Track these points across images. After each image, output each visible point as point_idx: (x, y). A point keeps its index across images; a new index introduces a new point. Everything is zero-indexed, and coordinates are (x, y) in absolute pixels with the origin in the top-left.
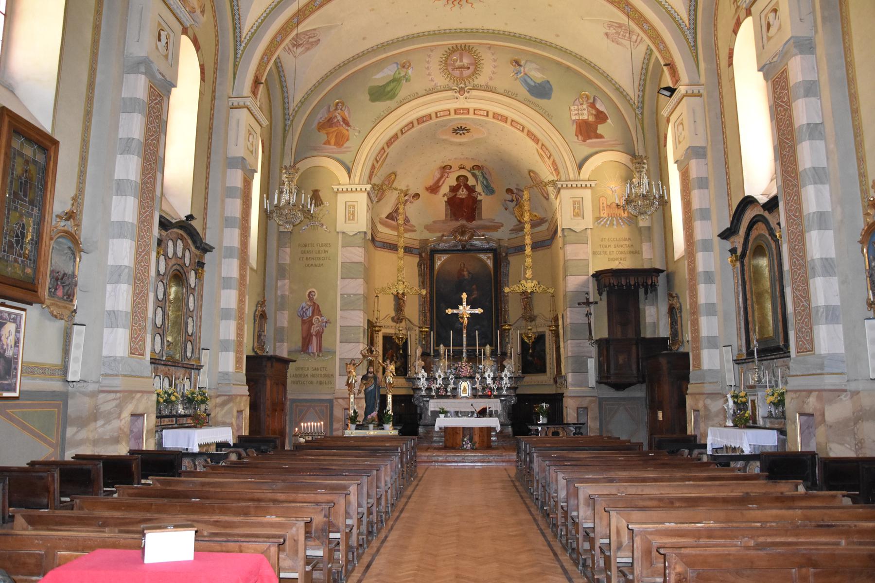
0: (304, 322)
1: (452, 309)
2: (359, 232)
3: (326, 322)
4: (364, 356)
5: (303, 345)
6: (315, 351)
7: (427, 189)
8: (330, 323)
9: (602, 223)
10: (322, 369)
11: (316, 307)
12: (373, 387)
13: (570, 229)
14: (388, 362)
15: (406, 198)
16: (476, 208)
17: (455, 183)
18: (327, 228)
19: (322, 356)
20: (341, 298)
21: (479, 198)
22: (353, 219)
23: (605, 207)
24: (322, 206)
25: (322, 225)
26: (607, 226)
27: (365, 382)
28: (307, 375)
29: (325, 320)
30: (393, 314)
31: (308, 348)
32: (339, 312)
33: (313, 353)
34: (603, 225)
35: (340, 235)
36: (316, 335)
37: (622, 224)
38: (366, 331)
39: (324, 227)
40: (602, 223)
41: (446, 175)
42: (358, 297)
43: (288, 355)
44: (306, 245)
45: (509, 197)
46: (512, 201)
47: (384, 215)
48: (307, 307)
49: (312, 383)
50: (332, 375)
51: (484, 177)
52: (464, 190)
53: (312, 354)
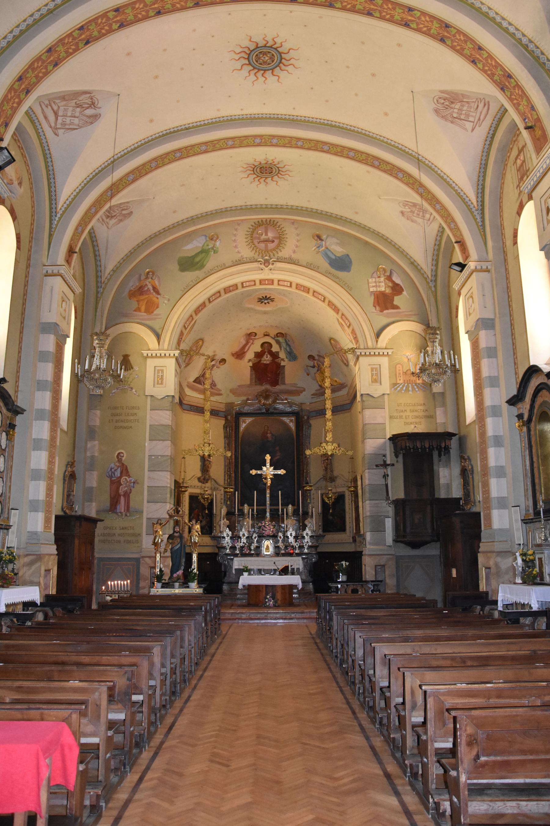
0: (112, 482)
1: (256, 470)
2: (167, 396)
3: (134, 483)
4: (171, 516)
5: (111, 505)
6: (123, 511)
7: (233, 355)
8: (138, 483)
9: (399, 389)
10: (130, 528)
11: (124, 468)
12: (177, 547)
13: (368, 394)
14: (194, 522)
15: (213, 363)
16: (279, 373)
17: (259, 349)
18: (136, 391)
19: (130, 516)
20: (149, 459)
21: (283, 364)
22: (162, 383)
23: (401, 374)
24: (132, 370)
25: (132, 388)
26: (403, 392)
27: (170, 541)
28: (114, 534)
29: (132, 481)
30: (199, 474)
31: (116, 508)
32: (147, 473)
33: (121, 513)
34: (398, 391)
35: (149, 398)
36: (124, 496)
37: (417, 390)
38: (173, 491)
39: (134, 390)
40: (399, 389)
41: (251, 341)
42: (165, 458)
43: (97, 514)
44: (115, 408)
45: (311, 363)
46: (314, 367)
47: (192, 379)
48: (116, 468)
49: (119, 542)
50: (139, 534)
51: (287, 344)
52: (269, 356)
53: (119, 514)
